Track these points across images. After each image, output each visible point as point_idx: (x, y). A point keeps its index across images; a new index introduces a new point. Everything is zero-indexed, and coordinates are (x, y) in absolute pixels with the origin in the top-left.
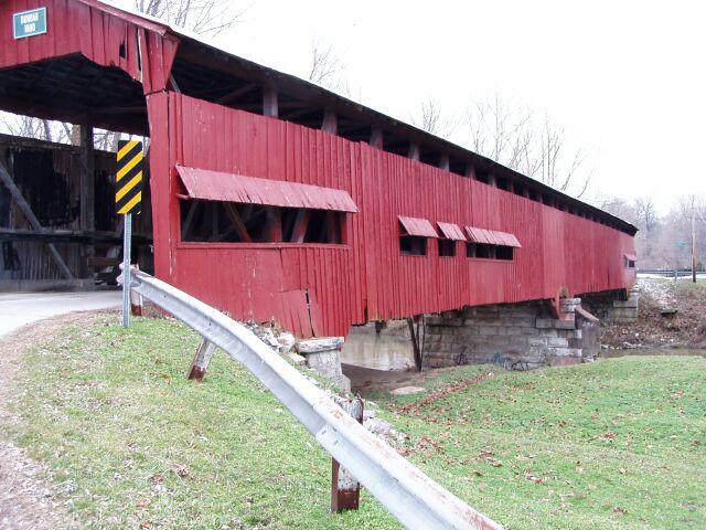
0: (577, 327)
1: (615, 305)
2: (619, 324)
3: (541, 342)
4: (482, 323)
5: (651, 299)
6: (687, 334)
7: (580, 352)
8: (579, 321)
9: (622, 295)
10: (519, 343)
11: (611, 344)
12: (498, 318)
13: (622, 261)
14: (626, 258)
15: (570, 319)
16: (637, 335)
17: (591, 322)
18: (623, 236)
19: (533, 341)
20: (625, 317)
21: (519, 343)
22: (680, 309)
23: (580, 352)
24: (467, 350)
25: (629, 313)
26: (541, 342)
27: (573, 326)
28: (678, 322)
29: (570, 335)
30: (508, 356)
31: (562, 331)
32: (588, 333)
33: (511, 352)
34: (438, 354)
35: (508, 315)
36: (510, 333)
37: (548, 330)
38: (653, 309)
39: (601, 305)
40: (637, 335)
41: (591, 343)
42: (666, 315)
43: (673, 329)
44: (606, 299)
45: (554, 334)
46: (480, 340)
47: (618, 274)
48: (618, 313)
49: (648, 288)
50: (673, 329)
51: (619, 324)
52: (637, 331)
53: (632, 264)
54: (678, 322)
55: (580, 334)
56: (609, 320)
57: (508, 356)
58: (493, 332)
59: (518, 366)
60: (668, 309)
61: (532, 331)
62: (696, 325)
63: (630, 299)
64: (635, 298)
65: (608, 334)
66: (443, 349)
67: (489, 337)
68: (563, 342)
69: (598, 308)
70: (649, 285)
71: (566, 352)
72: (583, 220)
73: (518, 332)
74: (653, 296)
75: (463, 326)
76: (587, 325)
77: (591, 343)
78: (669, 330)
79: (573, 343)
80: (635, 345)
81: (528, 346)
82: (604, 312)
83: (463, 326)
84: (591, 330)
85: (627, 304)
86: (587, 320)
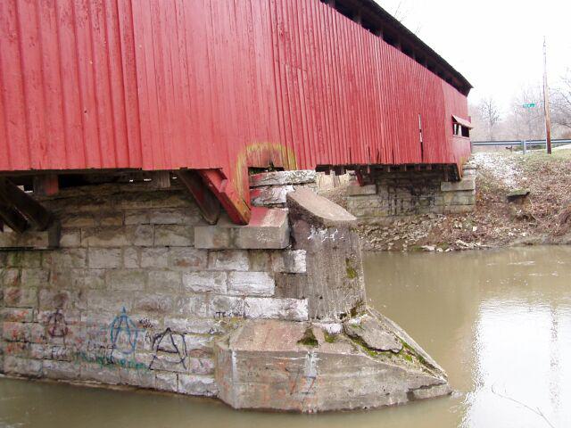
0: (293, 241)
1: (443, 188)
2: (449, 214)
3: (211, 282)
4: (93, 241)
5: (492, 178)
6: (544, 224)
7: (302, 308)
8: (300, 225)
9: (451, 173)
10: (165, 287)
11: (439, 244)
12: (122, 229)
13: (448, 123)
14: (454, 120)
15: (275, 222)
16: (475, 229)
17: (330, 226)
18: (449, 90)
19: (194, 281)
20: (458, 204)
21: (165, 287)
22: (533, 190)
23: (302, 308)
24: (67, 303)
25: (463, 199)
26: (211, 282)
27: (281, 240)
28: (531, 208)
29: (278, 265)
30: (143, 316)
31: (259, 255)
32: (320, 256)
33: (150, 309)
34: (17, 312)
35: (142, 219)
36: (148, 261)
37: (226, 252)
38: (496, 191)
39: (424, 189)
40: (475, 229)
41: (331, 285)
42: (515, 198)
43: (525, 217)
44: (414, 177)
45: (240, 263)
46: (88, 281)
47: (440, 138)
48: (448, 199)
49: (488, 164)
50: (525, 217)
51: (449, 214)
52: (474, 223)
53: (466, 131)
54: (531, 208)
55: (300, 260)
56: (435, 209)
57: (143, 316)
58: (110, 260)
59: (165, 342)
60: (517, 190)
61: (189, 256)
62: (556, 211)
63: (464, 179)
64: (470, 178)
65: (436, 231)
66: (23, 300)
67: (108, 273)
68: (260, 281)
69: (421, 193)
70: (489, 164)
71: (268, 307)
72: (376, 42)
73: (162, 261)
74: (495, 173)
75: (56, 247)
76: (319, 236)
77: (331, 285)
78: (520, 219)
79: (287, 285)
80: (471, 245)
81: (184, 293)
82: (430, 199)
83: (56, 247)
84: (329, 247)
85: (459, 187)
86: (317, 222)
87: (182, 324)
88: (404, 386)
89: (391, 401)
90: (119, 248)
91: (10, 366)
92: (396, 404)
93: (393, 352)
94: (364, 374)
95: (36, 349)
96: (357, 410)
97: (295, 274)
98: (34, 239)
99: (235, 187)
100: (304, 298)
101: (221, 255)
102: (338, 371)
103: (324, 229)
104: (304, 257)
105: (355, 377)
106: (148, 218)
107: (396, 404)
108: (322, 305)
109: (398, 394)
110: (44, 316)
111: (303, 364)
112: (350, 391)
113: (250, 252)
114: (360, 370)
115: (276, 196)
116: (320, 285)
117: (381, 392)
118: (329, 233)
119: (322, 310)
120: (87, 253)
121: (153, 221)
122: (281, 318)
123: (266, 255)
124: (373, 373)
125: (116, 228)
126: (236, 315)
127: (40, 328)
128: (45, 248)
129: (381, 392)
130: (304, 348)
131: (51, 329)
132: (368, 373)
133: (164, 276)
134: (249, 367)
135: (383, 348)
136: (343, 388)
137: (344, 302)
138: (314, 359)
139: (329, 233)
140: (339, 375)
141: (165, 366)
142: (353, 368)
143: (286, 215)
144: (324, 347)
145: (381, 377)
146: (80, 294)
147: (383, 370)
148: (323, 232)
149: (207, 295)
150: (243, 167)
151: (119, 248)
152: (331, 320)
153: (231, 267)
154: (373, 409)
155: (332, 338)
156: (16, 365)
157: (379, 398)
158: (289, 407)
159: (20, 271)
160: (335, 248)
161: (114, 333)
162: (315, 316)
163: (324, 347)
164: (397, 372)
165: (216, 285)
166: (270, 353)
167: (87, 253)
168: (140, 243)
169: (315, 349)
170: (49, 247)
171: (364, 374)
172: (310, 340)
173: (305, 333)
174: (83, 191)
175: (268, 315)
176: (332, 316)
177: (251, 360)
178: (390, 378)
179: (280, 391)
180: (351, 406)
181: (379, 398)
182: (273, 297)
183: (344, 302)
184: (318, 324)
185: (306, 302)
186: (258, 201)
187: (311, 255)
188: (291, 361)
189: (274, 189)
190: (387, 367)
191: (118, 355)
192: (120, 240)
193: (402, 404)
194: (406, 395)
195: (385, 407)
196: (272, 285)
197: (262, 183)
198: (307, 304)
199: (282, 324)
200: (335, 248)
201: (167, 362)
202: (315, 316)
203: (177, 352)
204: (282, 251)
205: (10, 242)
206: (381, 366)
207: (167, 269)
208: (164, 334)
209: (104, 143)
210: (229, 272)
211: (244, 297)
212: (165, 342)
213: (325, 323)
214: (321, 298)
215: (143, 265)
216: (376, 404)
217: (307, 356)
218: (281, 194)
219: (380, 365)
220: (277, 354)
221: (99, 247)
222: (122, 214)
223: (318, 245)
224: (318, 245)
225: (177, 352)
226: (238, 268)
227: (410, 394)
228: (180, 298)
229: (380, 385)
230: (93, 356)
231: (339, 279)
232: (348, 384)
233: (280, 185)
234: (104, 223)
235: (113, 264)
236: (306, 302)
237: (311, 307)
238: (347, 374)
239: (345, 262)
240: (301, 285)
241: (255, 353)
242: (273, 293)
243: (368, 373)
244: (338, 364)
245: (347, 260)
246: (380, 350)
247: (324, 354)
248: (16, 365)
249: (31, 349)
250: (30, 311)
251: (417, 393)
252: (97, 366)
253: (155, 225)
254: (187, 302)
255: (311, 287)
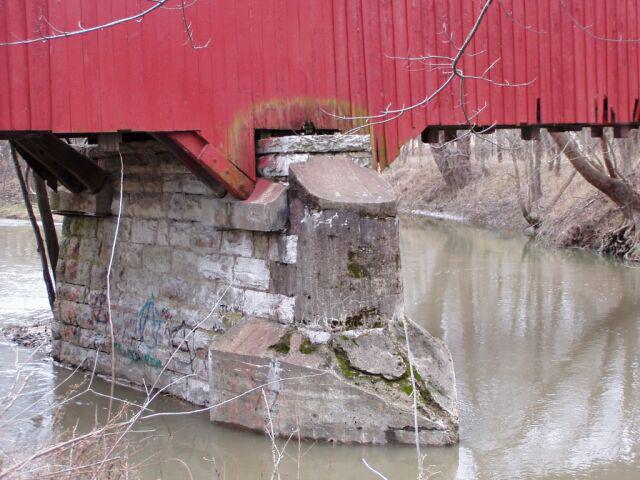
7: (287, 308)
12: (158, 197)
15: (269, 197)
19: (208, 267)
23: (287, 308)
37: (230, 231)
59: (178, 338)
73: (180, 238)
76: (312, 219)
79: (281, 279)
87: (192, 316)
88: (383, 423)
89: (363, 438)
90: (155, 219)
91: (65, 354)
92: (370, 443)
93: (383, 378)
94: (330, 396)
95: (84, 333)
96: (322, 441)
97: (286, 264)
98: (86, 204)
99: (226, 152)
100: (292, 296)
101: (231, 236)
102: (302, 388)
103: (319, 212)
104: (296, 244)
105: (321, 399)
106: (181, 185)
107: (370, 443)
108: (309, 307)
109: (373, 430)
110: (92, 297)
111: (267, 373)
112: (315, 416)
113: (254, 234)
114: (326, 390)
115: (279, 167)
116: (308, 281)
117: (350, 424)
118: (325, 217)
119: (310, 313)
120: (131, 224)
121: (185, 190)
122: (270, 320)
123: (264, 239)
124: (342, 397)
125: (153, 195)
126: (236, 310)
127: (88, 309)
128: (93, 214)
129: (350, 424)
130: (271, 354)
131: (96, 313)
132: (336, 397)
133: (184, 258)
134: (222, 371)
135: (371, 371)
136: (306, 411)
137: (341, 306)
138: (277, 369)
139: (325, 217)
140: (302, 393)
141: (177, 366)
142: (318, 386)
143: (284, 189)
144: (294, 356)
145: (351, 404)
146: (122, 274)
147: (354, 396)
148: (317, 215)
149: (217, 283)
150: (244, 129)
151: (155, 219)
152: (320, 327)
153: (237, 251)
154: (340, 443)
155: (309, 347)
156: (69, 354)
157: (348, 431)
158: (253, 426)
159: (79, 240)
160: (332, 237)
161: (143, 322)
162: (301, 320)
163: (294, 356)
164: (371, 401)
165: (222, 272)
166: (239, 355)
167: (131, 224)
168: (172, 215)
169: (282, 358)
170: (97, 213)
171: (330, 396)
172: (283, 347)
173: (282, 338)
174: (132, 148)
175: (260, 313)
176: (321, 323)
177: (223, 362)
178: (364, 409)
179: (247, 404)
180: (315, 435)
181: (348, 431)
182: (268, 291)
183: (341, 306)
184: (303, 329)
185: (293, 300)
186: (266, 171)
187: (302, 242)
188: (256, 368)
189: (279, 158)
190: (360, 393)
191: (143, 349)
192: (156, 211)
193: (378, 445)
194: (384, 434)
195: (356, 444)
196: (267, 277)
197: (269, 150)
198: (293, 302)
199: (269, 324)
200: (332, 237)
201: (179, 362)
202: (301, 320)
203: (188, 351)
204: (278, 234)
205: (68, 205)
206: (351, 390)
207: (189, 250)
208: (180, 328)
209: (343, 48)
210: (236, 256)
211: (245, 289)
212: (178, 338)
213: (311, 329)
214: (309, 298)
215: (173, 242)
216: (345, 438)
217: (271, 365)
218: (284, 164)
219: (351, 389)
220: (245, 358)
221: (142, 217)
222: (158, 179)
223: (311, 230)
224: (311, 230)
225: (188, 351)
226: (243, 253)
227: (390, 434)
228: (195, 285)
229: (351, 414)
230: (126, 348)
231: (334, 277)
232: (312, 406)
233: (285, 154)
234: (148, 189)
235: (150, 240)
236: (293, 300)
237: (297, 308)
238: (311, 394)
239: (346, 256)
240: (291, 279)
241: (227, 354)
242: (267, 287)
243: (336, 397)
244: (302, 379)
245: (351, 255)
246: (364, 372)
247: (288, 365)
248: (69, 354)
249: (80, 335)
250: (82, 289)
251: (400, 434)
252: (127, 360)
253: (187, 194)
254: (200, 290)
255: (299, 283)
